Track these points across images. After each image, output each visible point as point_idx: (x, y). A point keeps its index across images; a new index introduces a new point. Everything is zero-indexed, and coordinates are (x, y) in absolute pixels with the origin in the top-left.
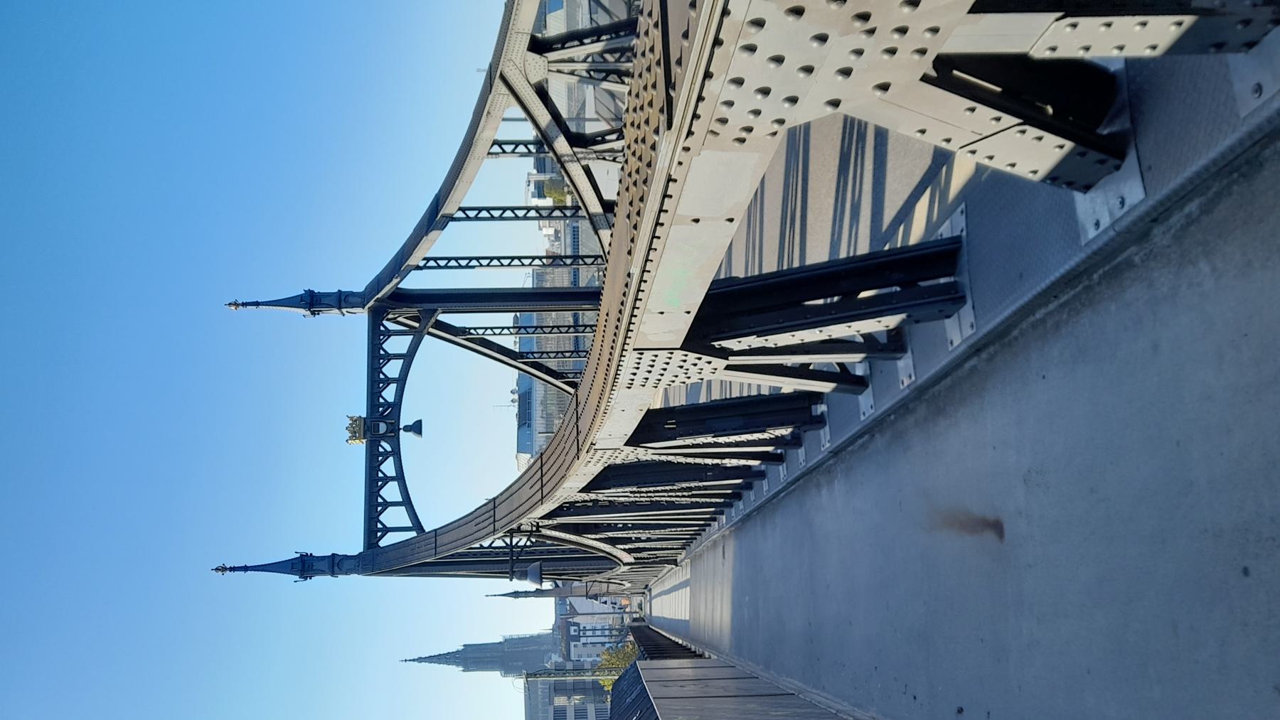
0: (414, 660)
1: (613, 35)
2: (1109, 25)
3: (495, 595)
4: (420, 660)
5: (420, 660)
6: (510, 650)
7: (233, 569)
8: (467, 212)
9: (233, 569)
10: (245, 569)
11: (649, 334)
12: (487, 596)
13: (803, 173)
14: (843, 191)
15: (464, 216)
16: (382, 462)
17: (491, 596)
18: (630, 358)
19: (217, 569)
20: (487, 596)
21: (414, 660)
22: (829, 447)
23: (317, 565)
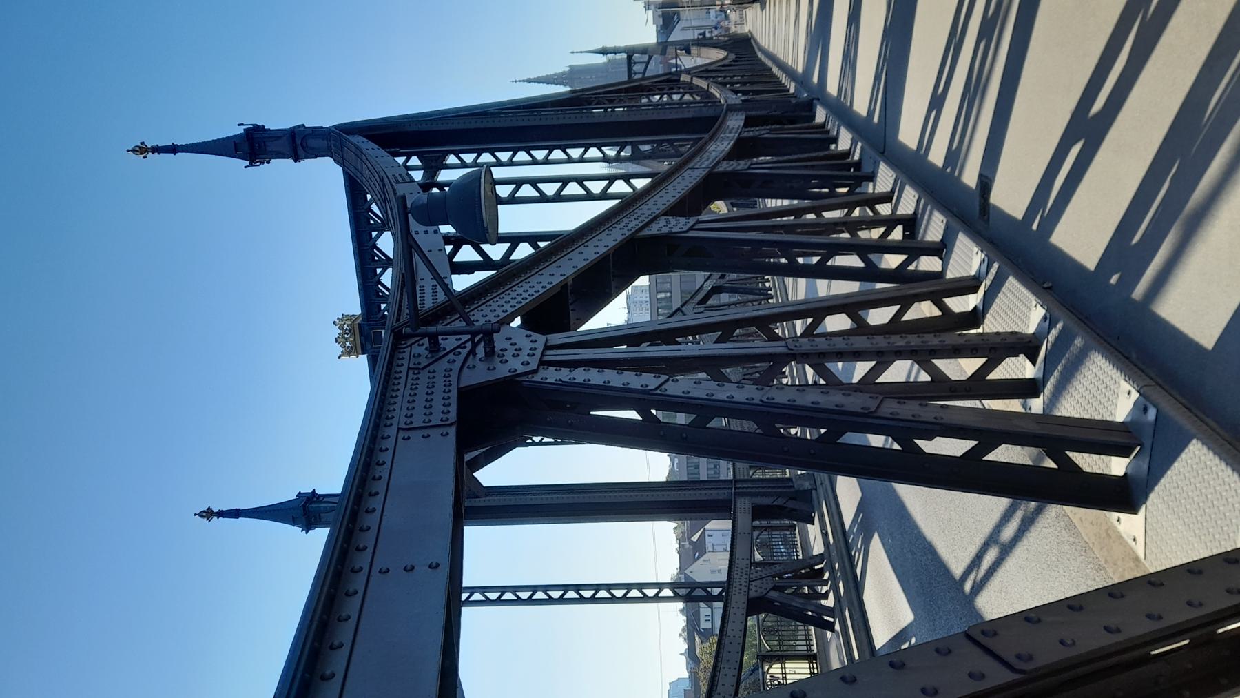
0: (524, 81)
1: (820, 115)
2: (737, 662)
3: (581, 52)
4: (529, 81)
5: (529, 81)
6: (614, 70)
7: (157, 150)
8: (582, 192)
9: (157, 150)
10: (173, 149)
11: (766, 594)
12: (573, 53)
13: (934, 121)
14: (897, 197)
15: (583, 192)
16: (378, 236)
17: (577, 52)
18: (453, 416)
19: (134, 151)
20: (573, 53)
21: (524, 81)
22: (739, 87)
23: (271, 147)
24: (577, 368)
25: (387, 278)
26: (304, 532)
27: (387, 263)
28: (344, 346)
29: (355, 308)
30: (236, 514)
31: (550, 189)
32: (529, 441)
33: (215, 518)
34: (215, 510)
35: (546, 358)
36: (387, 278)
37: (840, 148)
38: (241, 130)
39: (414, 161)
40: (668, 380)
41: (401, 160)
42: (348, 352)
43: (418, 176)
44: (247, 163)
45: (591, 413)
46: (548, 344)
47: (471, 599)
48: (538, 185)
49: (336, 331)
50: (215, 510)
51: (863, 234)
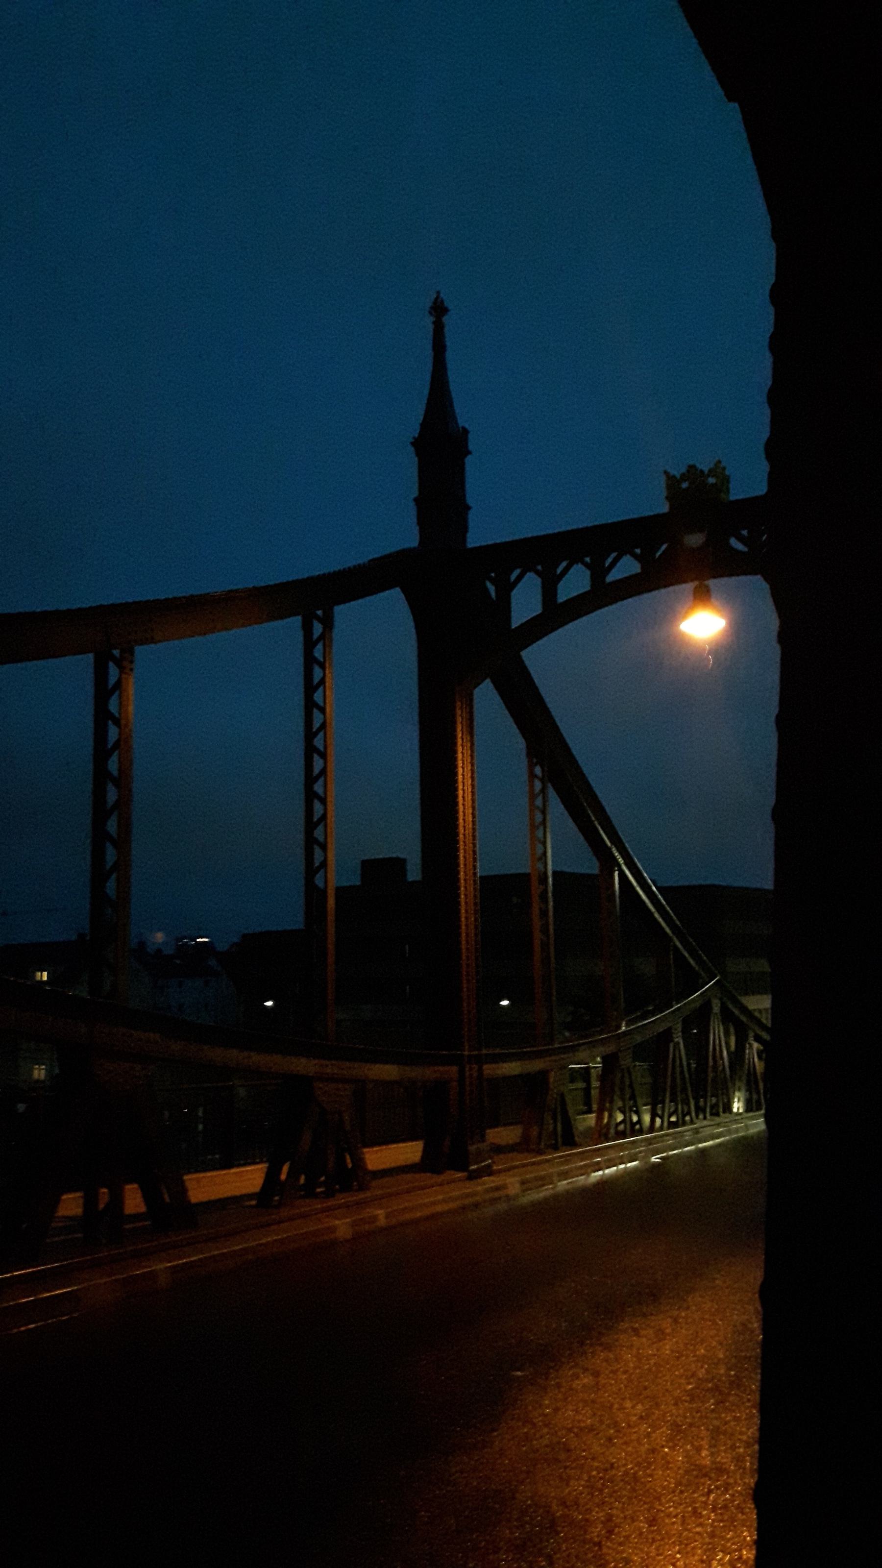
33: (433, 319)
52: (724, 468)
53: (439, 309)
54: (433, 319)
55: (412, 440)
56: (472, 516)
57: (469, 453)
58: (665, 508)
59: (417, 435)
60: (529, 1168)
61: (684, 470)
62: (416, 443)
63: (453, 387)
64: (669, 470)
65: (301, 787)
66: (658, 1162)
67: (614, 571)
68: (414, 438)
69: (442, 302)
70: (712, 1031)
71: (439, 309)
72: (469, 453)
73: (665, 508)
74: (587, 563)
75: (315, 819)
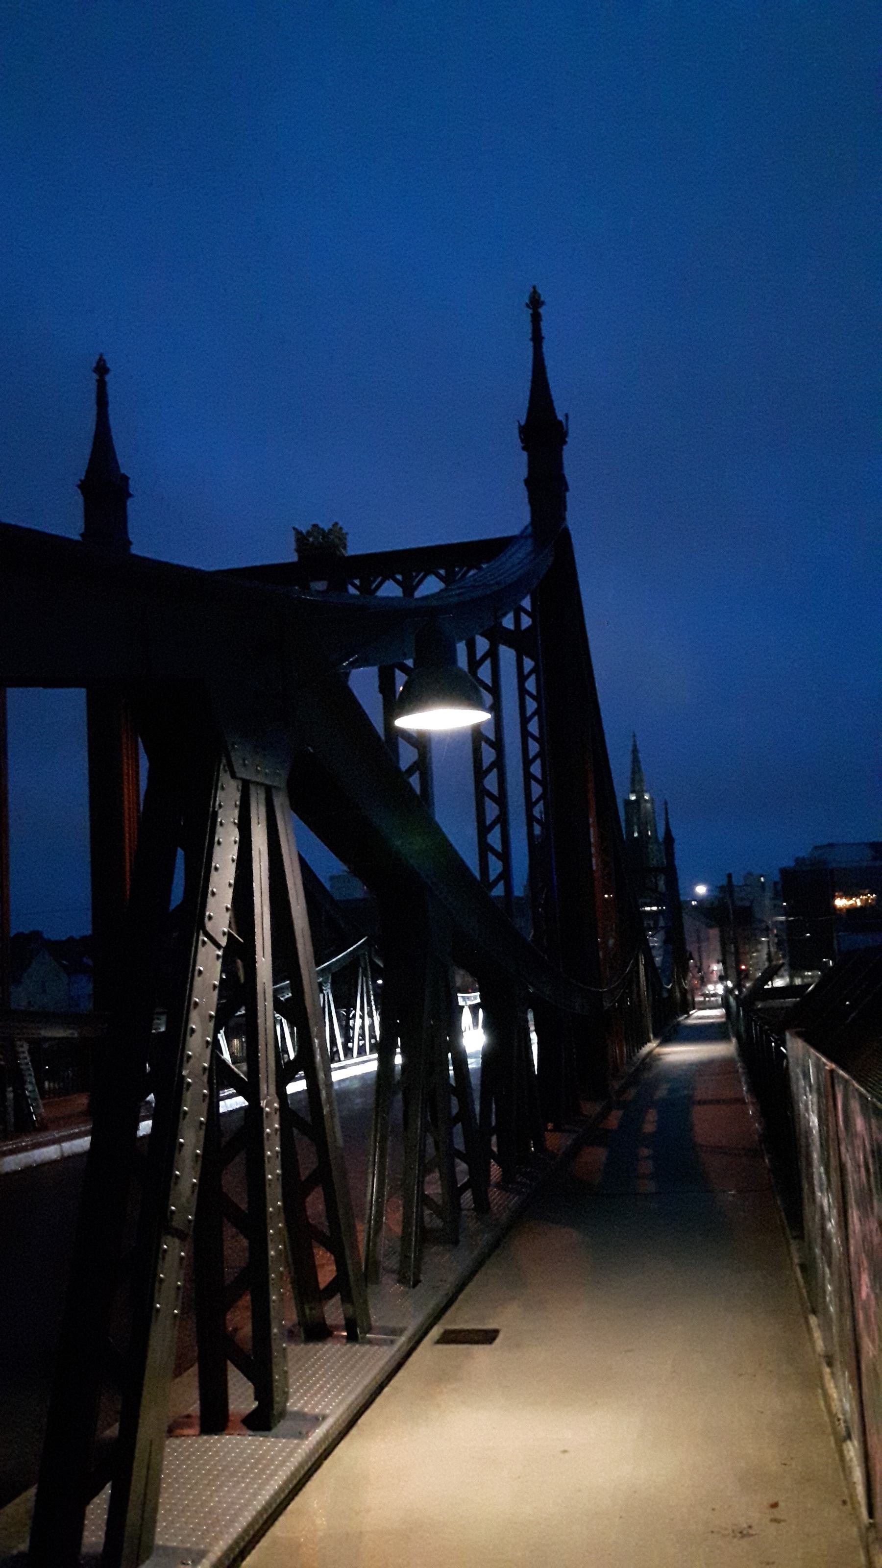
7: (536, 319)
9: (536, 319)
24: (239, 828)
25: (390, 590)
26: (79, 483)
27: (409, 588)
28: (309, 533)
29: (355, 547)
30: (537, 338)
31: (491, 782)
32: (415, 781)
33: (531, 311)
34: (541, 310)
35: (253, 789)
36: (390, 590)
37: (547, 1135)
38: (560, 417)
39: (526, 622)
40: (219, 946)
41: (526, 603)
42: (301, 539)
43: (508, 622)
44: (523, 423)
45: (180, 852)
46: (274, 791)
47: (527, 698)
48: (495, 770)
49: (326, 526)
50: (541, 310)
51: (463, 1179)
52: (341, 528)
53: (535, 302)
54: (531, 311)
55: (79, 483)
56: (571, 497)
57: (130, 495)
58: (294, 558)
59: (83, 478)
60: (837, 1151)
61: (309, 528)
62: (83, 486)
63: (550, 374)
64: (297, 527)
65: (518, 727)
66: (474, 1109)
67: (421, 587)
68: (81, 480)
69: (539, 296)
70: (359, 987)
71: (535, 302)
72: (130, 495)
73: (294, 558)
74: (442, 575)
75: (531, 757)
